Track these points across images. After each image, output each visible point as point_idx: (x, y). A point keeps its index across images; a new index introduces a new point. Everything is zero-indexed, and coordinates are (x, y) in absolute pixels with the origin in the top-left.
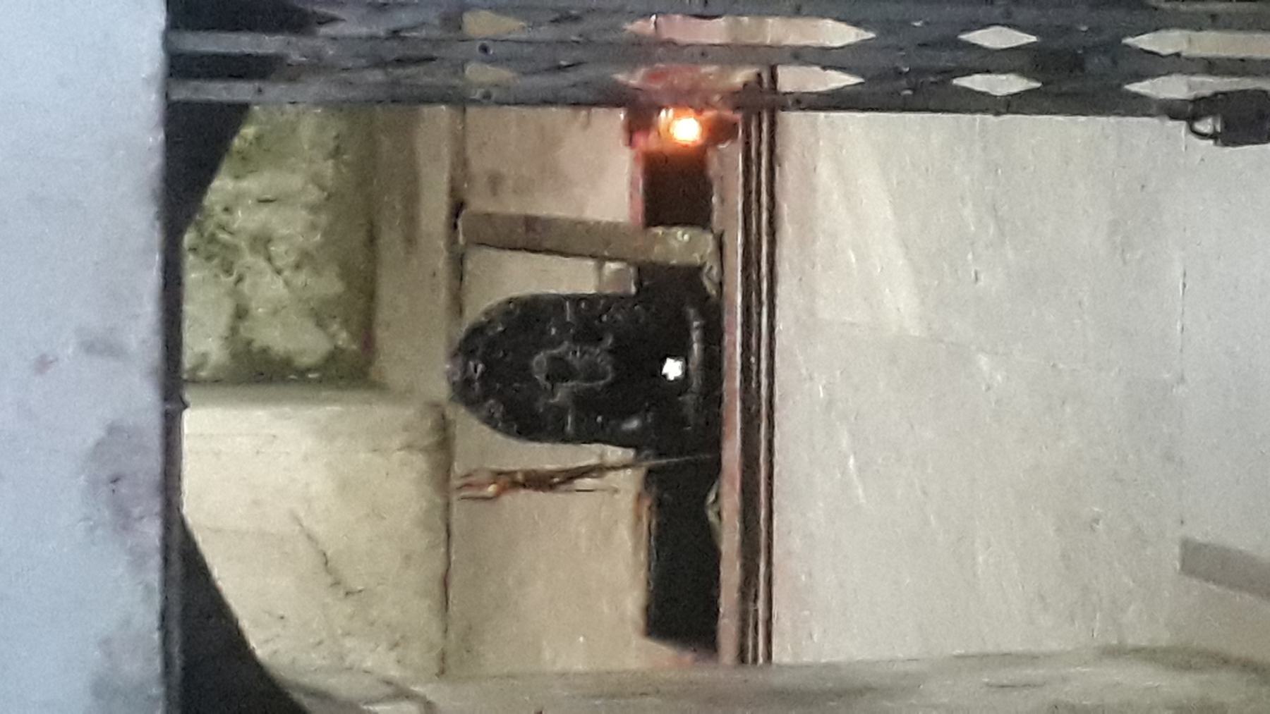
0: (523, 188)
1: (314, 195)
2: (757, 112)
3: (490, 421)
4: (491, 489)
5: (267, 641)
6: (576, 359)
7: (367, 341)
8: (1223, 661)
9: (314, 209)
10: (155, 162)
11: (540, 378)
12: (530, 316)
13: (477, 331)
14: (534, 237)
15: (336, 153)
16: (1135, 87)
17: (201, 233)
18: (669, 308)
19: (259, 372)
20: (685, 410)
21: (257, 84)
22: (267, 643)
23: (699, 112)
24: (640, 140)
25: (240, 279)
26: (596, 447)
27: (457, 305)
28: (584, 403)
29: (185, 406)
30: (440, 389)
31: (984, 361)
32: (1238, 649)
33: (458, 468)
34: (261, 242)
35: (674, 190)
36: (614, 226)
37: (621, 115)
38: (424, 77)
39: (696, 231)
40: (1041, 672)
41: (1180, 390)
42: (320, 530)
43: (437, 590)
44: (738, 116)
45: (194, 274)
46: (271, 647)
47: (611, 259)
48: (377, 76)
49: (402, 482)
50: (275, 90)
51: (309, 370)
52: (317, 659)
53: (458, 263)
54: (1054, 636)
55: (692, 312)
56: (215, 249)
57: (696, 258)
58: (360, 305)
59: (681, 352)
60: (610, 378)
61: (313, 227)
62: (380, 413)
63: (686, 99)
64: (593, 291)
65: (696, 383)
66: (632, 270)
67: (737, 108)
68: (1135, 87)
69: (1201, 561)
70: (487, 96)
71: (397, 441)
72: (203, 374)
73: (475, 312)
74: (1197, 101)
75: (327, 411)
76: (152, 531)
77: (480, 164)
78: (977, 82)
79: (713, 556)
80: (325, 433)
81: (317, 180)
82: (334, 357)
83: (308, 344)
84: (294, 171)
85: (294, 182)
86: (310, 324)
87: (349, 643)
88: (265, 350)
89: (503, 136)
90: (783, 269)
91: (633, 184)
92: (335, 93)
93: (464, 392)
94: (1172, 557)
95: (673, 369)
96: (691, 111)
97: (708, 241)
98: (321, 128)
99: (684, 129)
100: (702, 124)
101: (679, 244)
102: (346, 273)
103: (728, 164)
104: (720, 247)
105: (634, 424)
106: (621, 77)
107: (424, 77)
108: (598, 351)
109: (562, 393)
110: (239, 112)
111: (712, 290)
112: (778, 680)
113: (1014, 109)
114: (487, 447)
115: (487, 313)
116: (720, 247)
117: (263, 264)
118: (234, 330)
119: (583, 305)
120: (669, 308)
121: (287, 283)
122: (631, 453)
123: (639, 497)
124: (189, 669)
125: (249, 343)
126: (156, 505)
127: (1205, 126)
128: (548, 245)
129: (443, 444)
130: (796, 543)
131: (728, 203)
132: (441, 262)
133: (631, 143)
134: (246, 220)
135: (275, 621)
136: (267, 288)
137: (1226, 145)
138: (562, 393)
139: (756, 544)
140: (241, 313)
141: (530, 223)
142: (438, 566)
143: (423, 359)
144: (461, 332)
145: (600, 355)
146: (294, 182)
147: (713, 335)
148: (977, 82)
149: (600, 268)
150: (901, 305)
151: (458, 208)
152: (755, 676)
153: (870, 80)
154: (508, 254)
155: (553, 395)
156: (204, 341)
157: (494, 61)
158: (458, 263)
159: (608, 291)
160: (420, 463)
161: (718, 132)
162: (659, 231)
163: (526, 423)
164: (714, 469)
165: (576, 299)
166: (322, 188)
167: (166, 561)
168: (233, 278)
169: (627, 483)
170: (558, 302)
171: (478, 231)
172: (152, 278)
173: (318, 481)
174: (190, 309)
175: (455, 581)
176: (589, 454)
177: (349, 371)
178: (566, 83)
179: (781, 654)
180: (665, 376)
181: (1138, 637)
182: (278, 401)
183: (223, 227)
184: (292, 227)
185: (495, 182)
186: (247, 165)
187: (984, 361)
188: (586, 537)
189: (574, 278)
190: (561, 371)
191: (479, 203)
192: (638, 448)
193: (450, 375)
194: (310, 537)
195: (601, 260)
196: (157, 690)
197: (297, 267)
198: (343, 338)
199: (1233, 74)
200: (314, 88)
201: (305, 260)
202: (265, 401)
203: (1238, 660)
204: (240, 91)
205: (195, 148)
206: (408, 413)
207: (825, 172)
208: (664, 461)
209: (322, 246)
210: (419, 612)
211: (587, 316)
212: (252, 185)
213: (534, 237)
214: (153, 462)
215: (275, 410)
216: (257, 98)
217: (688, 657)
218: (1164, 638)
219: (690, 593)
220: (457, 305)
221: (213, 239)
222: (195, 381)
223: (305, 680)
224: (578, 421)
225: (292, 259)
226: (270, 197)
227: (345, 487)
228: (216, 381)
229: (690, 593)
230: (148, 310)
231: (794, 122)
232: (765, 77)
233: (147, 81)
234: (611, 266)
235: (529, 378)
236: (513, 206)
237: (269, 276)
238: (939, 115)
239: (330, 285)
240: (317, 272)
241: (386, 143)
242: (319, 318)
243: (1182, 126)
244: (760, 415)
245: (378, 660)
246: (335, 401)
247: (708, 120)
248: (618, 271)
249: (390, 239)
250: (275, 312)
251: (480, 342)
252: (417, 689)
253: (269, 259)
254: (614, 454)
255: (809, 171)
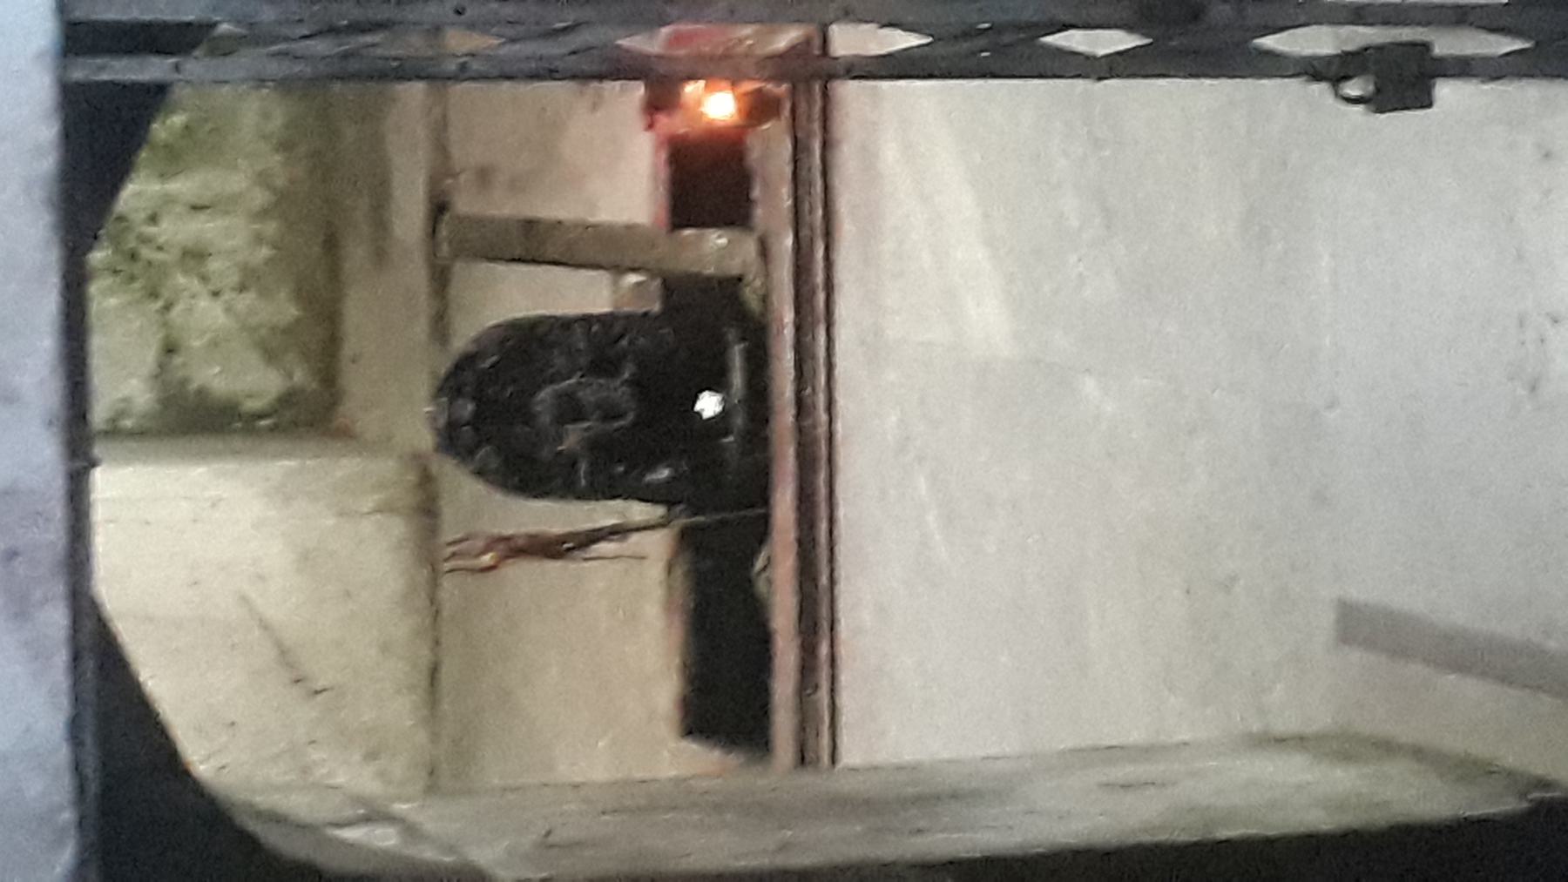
0: (517, 185)
1: (260, 198)
2: (805, 87)
3: (480, 473)
4: (487, 559)
5: (209, 757)
6: (590, 394)
7: (329, 377)
8: (1386, 748)
9: (263, 214)
10: (48, 163)
11: (545, 419)
12: (529, 343)
13: (465, 362)
14: (534, 244)
15: (285, 146)
16: (1269, 42)
17: (117, 250)
18: (705, 327)
19: (193, 420)
20: (727, 455)
21: (172, 60)
22: (204, 757)
23: (734, 84)
24: (663, 120)
25: (168, 307)
26: (618, 504)
27: (440, 326)
28: (601, 448)
29: (94, 464)
30: (425, 439)
31: (1090, 386)
32: (1406, 732)
33: (449, 532)
34: (194, 256)
35: (706, 182)
36: (630, 228)
37: (638, 90)
38: (379, 45)
39: (735, 233)
40: (1162, 767)
41: (1331, 416)
42: (273, 613)
43: (425, 683)
44: (784, 88)
45: (104, 299)
46: (215, 763)
47: (634, 270)
48: (321, 46)
49: (376, 552)
50: (196, 66)
51: (261, 416)
52: (277, 773)
53: (440, 279)
54: (1183, 723)
55: (731, 335)
56: (137, 268)
57: (734, 267)
58: (319, 338)
59: (717, 383)
60: (631, 417)
61: (259, 239)
62: (346, 466)
63: (716, 68)
64: (606, 309)
65: (739, 421)
66: (657, 282)
67: (777, 78)
68: (1269, 42)
69: (1361, 627)
70: (463, 67)
71: (368, 503)
72: (128, 423)
73: (464, 335)
74: (1346, 57)
75: (278, 467)
76: (55, 619)
77: (467, 154)
78: (1073, 40)
79: (763, 639)
80: (283, 495)
81: (263, 179)
82: (287, 400)
83: (256, 382)
84: (235, 168)
85: (236, 181)
86: (254, 358)
87: (315, 755)
88: (202, 392)
89: (493, 117)
90: (843, 275)
91: (655, 177)
92: (274, 68)
93: (452, 440)
94: (1325, 621)
95: (709, 404)
96: (724, 84)
97: (750, 247)
98: (266, 116)
99: (718, 106)
100: (738, 99)
101: (713, 248)
102: (303, 295)
103: (771, 151)
104: (764, 251)
105: (664, 473)
106: (625, 42)
107: (379, 45)
108: (618, 382)
109: (573, 438)
110: (154, 96)
111: (753, 303)
112: (842, 784)
113: (1337, 61)
114: (484, 508)
115: (477, 340)
116: (764, 251)
117: (195, 285)
118: (162, 367)
119: (595, 328)
120: (705, 327)
121: (228, 310)
122: (659, 511)
123: (670, 568)
124: (106, 793)
125: (184, 382)
126: (59, 588)
127: (1353, 89)
128: (550, 257)
129: (426, 508)
130: (867, 617)
131: (773, 201)
132: (417, 275)
133: (650, 126)
134: (175, 230)
135: (224, 732)
136: (205, 314)
137: (1381, 111)
138: (573, 438)
139: (816, 617)
140: (170, 349)
141: (530, 226)
142: (425, 654)
143: (401, 403)
144: (444, 366)
145: (617, 390)
146: (236, 181)
147: (759, 362)
148: (1073, 40)
149: (615, 283)
150: (988, 320)
151: (439, 208)
152: (808, 781)
153: (937, 39)
154: (501, 268)
155: (560, 439)
156: (122, 382)
157: (471, 26)
158: (440, 279)
159: (627, 309)
160: (398, 527)
161: (759, 109)
162: (688, 232)
163: (528, 474)
164: (761, 530)
165: (587, 320)
166: (269, 187)
167: (76, 658)
168: (160, 304)
169: (656, 546)
170: (565, 324)
171: (464, 239)
172: (48, 304)
173: (275, 554)
174: (98, 343)
175: (445, 672)
176: (605, 513)
177: (308, 416)
178: (564, 50)
179: (851, 755)
180: (699, 414)
181: (1285, 723)
182: (218, 455)
183: (145, 240)
184: (232, 237)
185: (484, 176)
186: (174, 160)
187: (1090, 386)
188: (607, 615)
189: (585, 294)
190: (570, 410)
191: (465, 204)
192: (670, 503)
193: (433, 418)
194: (265, 626)
195: (619, 269)
196: (68, 816)
197: (242, 288)
198: (300, 376)
199: (1386, 23)
200: (246, 61)
201: (249, 280)
202: (201, 456)
203: (432, 650)
204: (153, 69)
205: (101, 139)
206: (386, 467)
207: (890, 153)
208: (700, 519)
209: (269, 261)
210: (398, 710)
211: (600, 340)
212: (183, 186)
213: (534, 244)
214: (54, 535)
215: (217, 466)
216: (176, 76)
217: (734, 759)
218: (1321, 718)
219: (737, 679)
220: (440, 326)
221: (133, 256)
222: (113, 432)
223: (262, 801)
224: (591, 473)
225: (234, 279)
226: (201, 203)
227: (306, 559)
228: (139, 434)
229: (737, 679)
230: (45, 343)
231: (849, 92)
232: (817, 42)
233: (40, 56)
234: (633, 278)
235: (528, 418)
236: (504, 207)
237: (204, 303)
238: (902, 83)
239: (284, 309)
240: (264, 293)
241: (350, 132)
242: (270, 355)
243: (1321, 89)
244: (816, 458)
245: (353, 776)
246: (288, 455)
247: (746, 94)
248: (638, 284)
249: (356, 254)
250: (214, 344)
251: (468, 376)
252: (400, 808)
253: (204, 279)
254: (639, 511)
255: (869, 155)
